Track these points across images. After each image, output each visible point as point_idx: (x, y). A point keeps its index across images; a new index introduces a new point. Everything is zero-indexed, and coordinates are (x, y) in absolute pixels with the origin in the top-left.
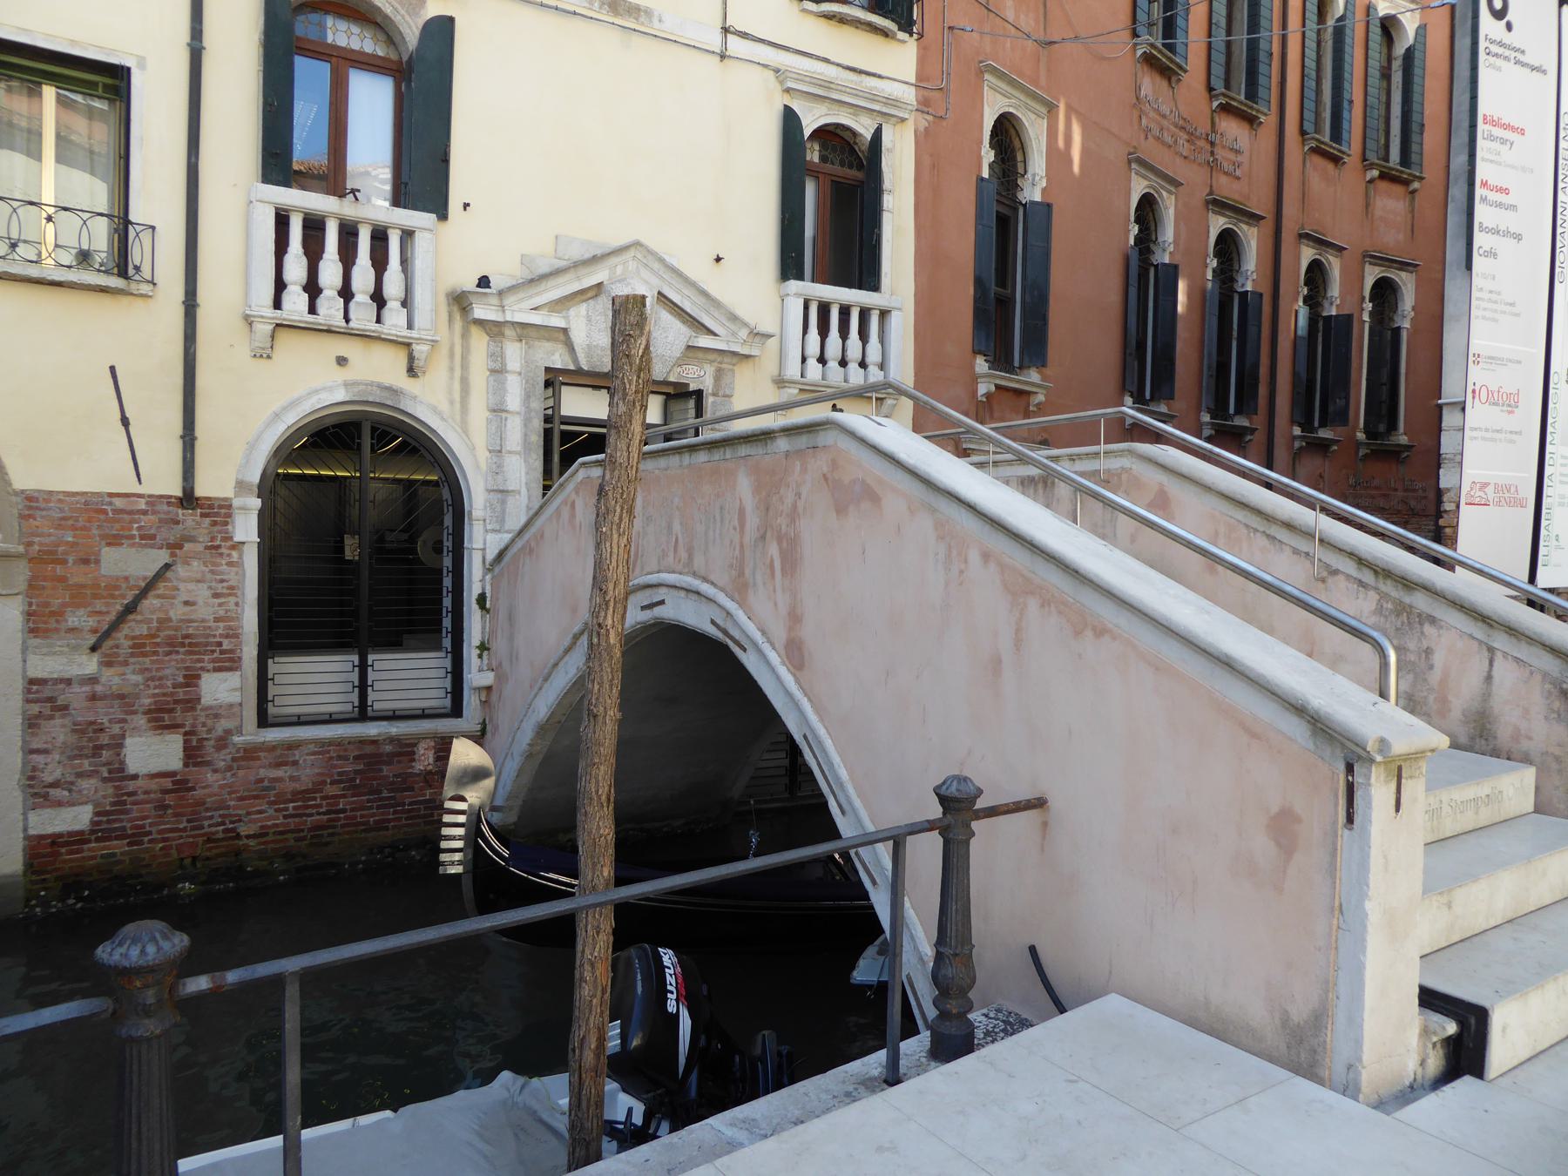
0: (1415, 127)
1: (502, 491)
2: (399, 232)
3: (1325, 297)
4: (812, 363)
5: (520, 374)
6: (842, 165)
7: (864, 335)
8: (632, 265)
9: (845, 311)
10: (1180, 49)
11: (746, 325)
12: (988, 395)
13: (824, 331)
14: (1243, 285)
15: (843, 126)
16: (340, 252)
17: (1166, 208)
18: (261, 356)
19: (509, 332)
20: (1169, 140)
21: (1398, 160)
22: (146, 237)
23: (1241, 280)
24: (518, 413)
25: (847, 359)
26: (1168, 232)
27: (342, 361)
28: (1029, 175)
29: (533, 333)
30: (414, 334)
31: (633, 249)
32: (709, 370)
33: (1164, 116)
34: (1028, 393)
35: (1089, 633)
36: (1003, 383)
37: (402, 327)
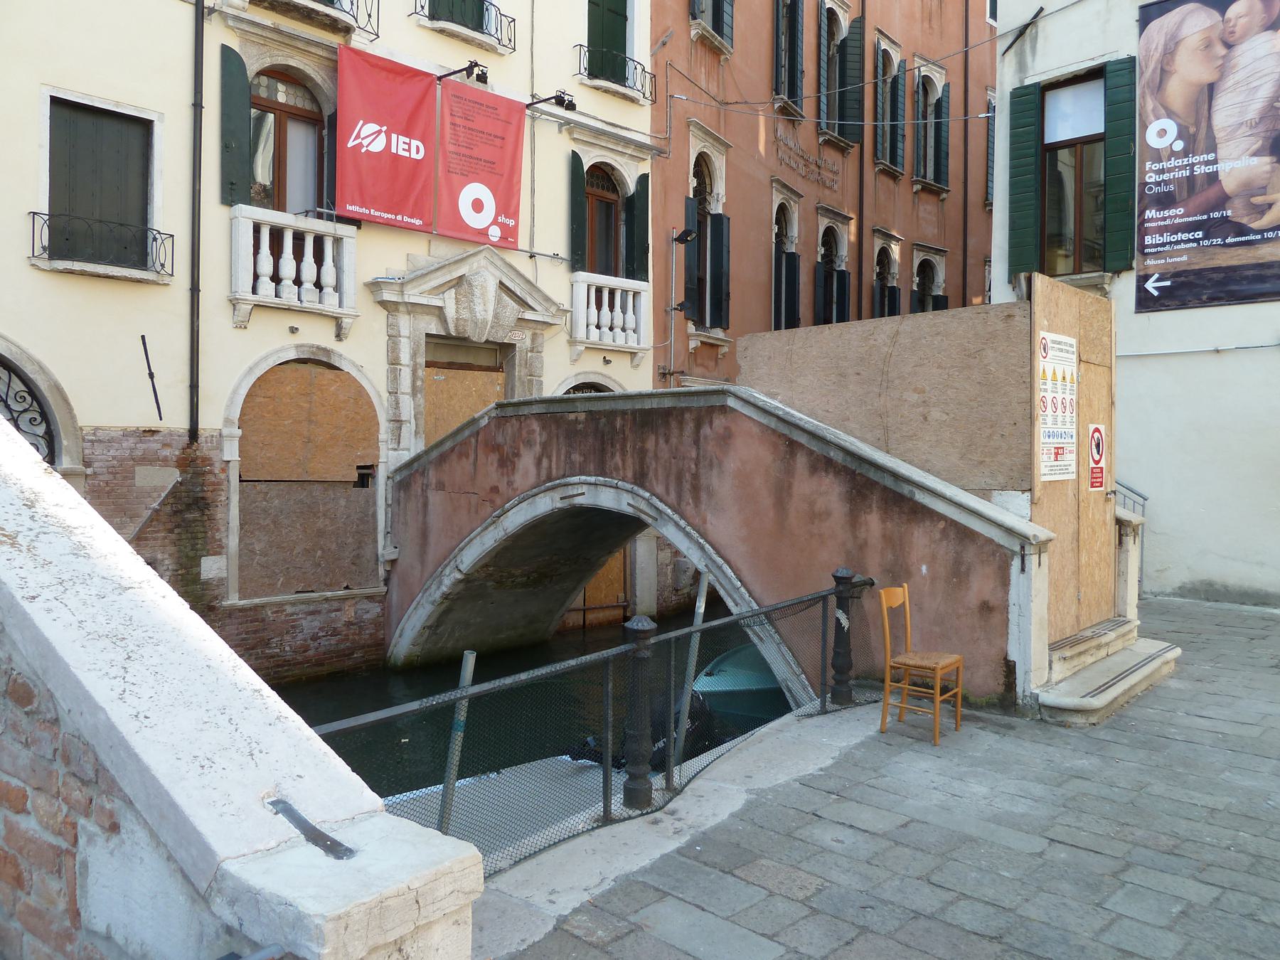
0: (943, 155)
1: (398, 421)
2: (332, 238)
3: (889, 273)
4: (593, 328)
5: (409, 338)
6: (598, 188)
7: (624, 311)
8: (483, 262)
9: (612, 292)
10: (799, 102)
11: (554, 303)
12: (695, 349)
13: (599, 306)
14: (839, 266)
15: (606, 163)
16: (294, 253)
17: (793, 213)
18: (241, 327)
19: (402, 308)
20: (794, 166)
21: (932, 178)
22: (168, 243)
23: (838, 262)
24: (408, 366)
25: (626, 326)
26: (795, 230)
27: (293, 330)
28: (714, 194)
29: (419, 309)
30: (344, 311)
31: (484, 252)
32: (528, 334)
33: (791, 149)
34: (718, 346)
35: (875, 498)
36: (705, 340)
37: (271, 296)
